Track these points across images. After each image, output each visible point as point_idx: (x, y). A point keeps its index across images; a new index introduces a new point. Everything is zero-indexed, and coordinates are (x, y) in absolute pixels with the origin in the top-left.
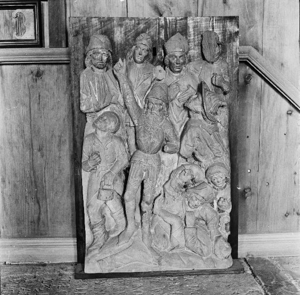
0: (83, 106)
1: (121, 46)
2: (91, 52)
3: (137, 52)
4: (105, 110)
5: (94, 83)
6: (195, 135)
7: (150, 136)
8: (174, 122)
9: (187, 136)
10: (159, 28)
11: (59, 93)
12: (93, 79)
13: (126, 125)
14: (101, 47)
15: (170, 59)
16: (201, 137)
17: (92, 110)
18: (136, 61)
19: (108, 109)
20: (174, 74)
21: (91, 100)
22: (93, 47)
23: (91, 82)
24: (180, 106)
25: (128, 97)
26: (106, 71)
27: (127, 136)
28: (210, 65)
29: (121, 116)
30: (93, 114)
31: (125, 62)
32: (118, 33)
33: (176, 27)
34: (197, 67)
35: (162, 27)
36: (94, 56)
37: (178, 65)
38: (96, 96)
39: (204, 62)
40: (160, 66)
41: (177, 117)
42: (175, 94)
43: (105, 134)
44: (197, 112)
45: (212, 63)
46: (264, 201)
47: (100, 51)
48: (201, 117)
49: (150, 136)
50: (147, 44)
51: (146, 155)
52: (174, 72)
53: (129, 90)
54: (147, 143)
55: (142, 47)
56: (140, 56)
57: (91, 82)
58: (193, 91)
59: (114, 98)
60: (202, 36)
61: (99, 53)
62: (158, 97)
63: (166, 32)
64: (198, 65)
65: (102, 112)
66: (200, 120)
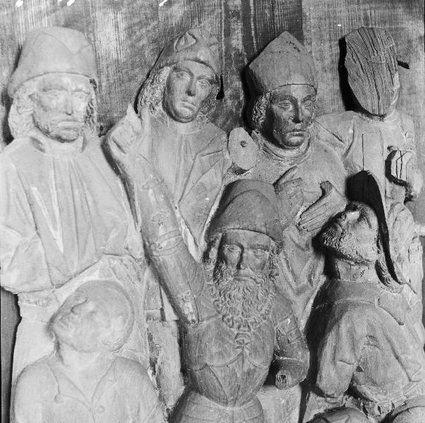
0: (10, 269)
1: (118, 70)
2: (33, 87)
3: (180, 85)
4: (86, 278)
5: (45, 190)
6: (362, 330)
7: (239, 351)
8: (290, 292)
9: (338, 334)
10: (228, 17)
11: (333, 173)
12: (42, 177)
13: (148, 317)
14: (68, 67)
15: (275, 107)
16: (379, 334)
17: (43, 281)
18: (175, 116)
19: (94, 276)
20: (280, 152)
21: (40, 247)
22: (41, 67)
23: (34, 189)
24: (303, 244)
25: (161, 231)
26: (83, 148)
27: (152, 349)
28: (375, 123)
29: (133, 291)
30: (45, 294)
31: (147, 119)
32: (110, 29)
33: (273, 17)
34: (339, 129)
35: (236, 14)
36: (45, 98)
37: (298, 126)
38: (57, 235)
39: (356, 116)
40: (242, 130)
41: (296, 278)
42: (293, 210)
43: (92, 361)
44: (362, 262)
45: (382, 117)
46: (275, 407)
47: (66, 80)
48: (372, 276)
49: (239, 351)
50: (212, 63)
51: (228, 409)
52: (285, 145)
53: (164, 209)
54: (235, 374)
55: (198, 69)
56: (191, 98)
57: (34, 189)
58: (336, 199)
59: (112, 236)
60: (342, 43)
61: (62, 88)
62: (259, 225)
63: (246, 30)
64: (342, 124)
65: (75, 284)
66: (371, 285)
